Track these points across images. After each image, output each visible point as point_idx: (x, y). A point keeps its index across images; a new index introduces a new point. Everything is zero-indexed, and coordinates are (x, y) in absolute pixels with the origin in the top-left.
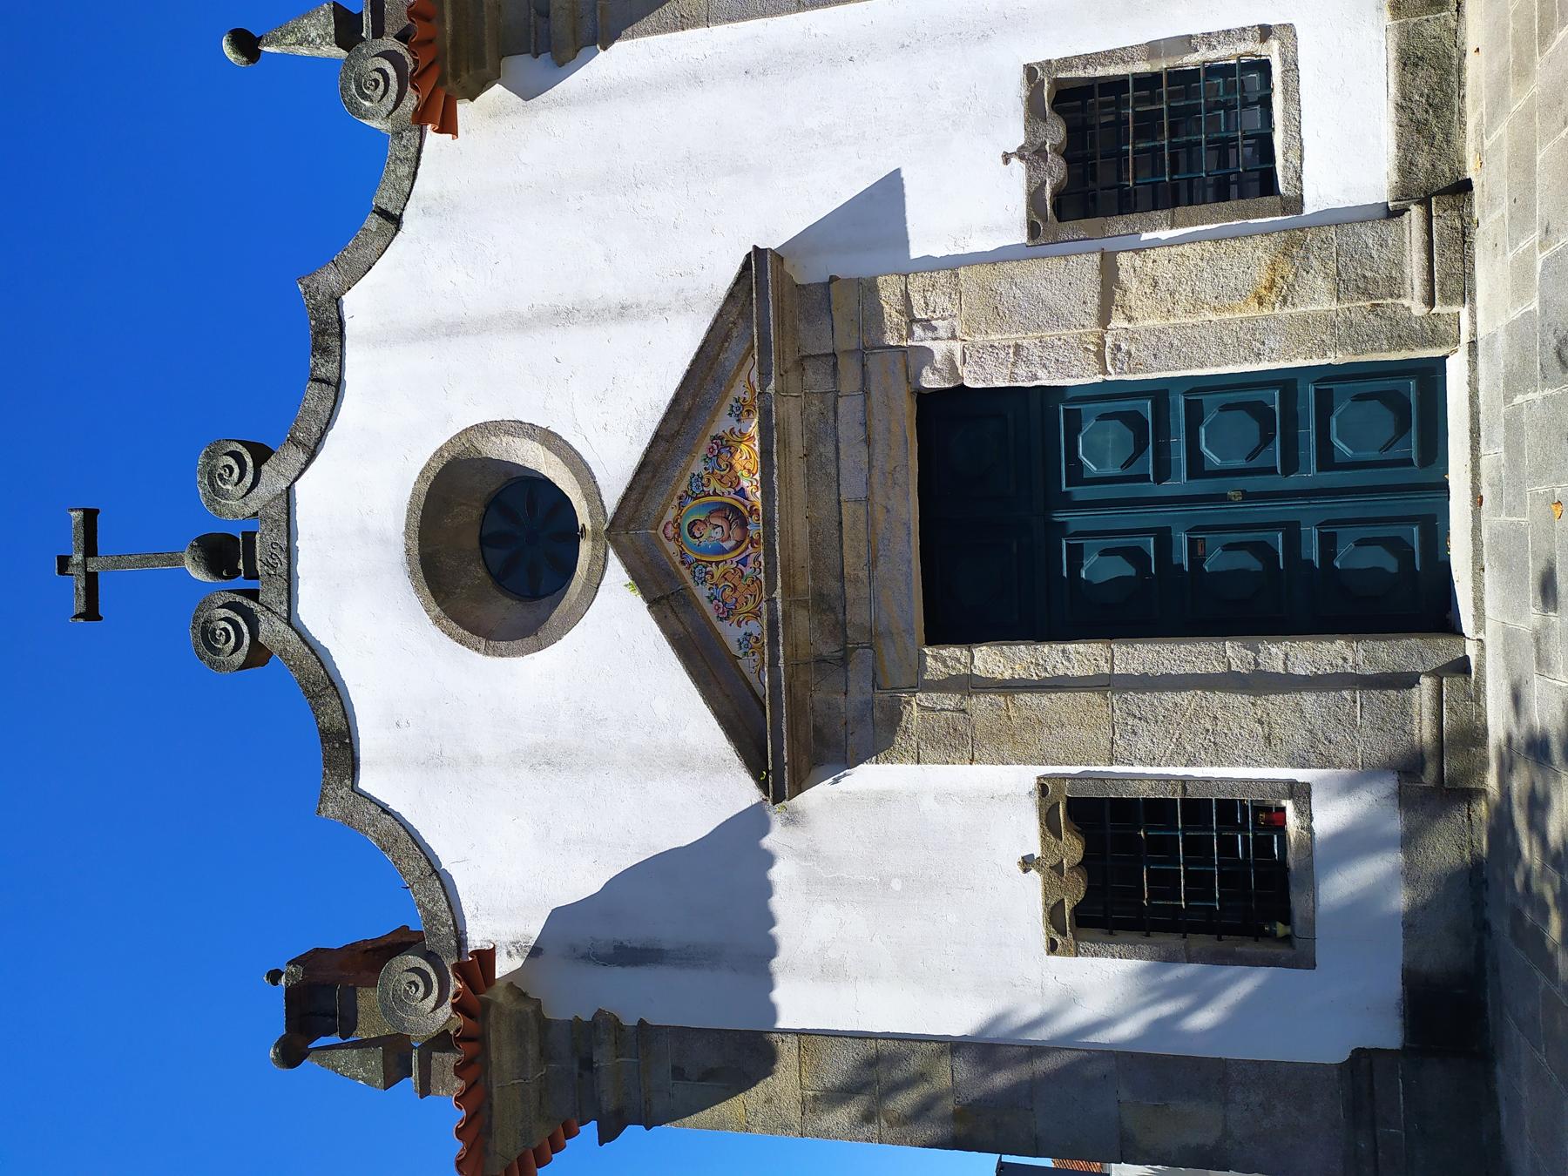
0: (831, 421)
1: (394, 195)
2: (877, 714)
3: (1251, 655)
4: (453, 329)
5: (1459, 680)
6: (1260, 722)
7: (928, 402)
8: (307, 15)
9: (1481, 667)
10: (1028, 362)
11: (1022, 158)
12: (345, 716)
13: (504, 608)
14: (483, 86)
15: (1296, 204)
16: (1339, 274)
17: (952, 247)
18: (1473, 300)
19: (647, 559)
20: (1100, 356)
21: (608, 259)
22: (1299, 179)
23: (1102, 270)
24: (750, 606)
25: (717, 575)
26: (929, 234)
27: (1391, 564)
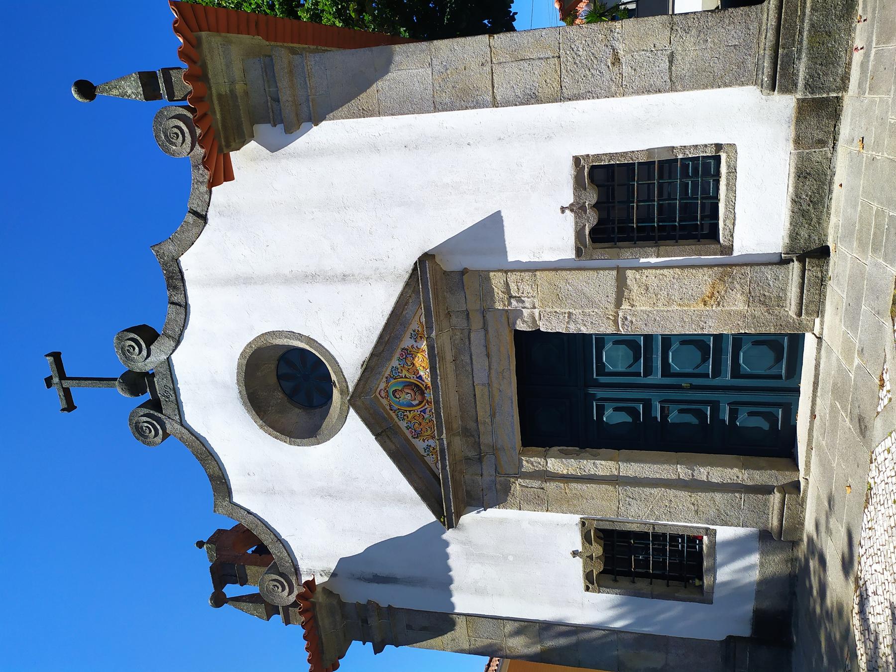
0: (467, 343)
1: (200, 203)
2: (498, 486)
3: (690, 472)
4: (247, 281)
5: (794, 496)
6: (693, 504)
7: (519, 335)
8: (123, 78)
9: (805, 491)
10: (575, 322)
11: (572, 211)
12: (220, 469)
13: (296, 416)
14: (244, 143)
15: (729, 249)
16: (750, 293)
17: (531, 256)
18: (823, 316)
19: (372, 411)
20: (616, 322)
21: (333, 248)
22: (732, 236)
23: (617, 280)
24: (429, 432)
25: (410, 417)
26: (519, 249)
27: (766, 426)
